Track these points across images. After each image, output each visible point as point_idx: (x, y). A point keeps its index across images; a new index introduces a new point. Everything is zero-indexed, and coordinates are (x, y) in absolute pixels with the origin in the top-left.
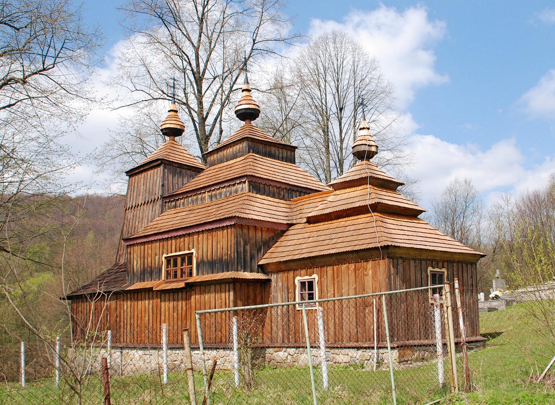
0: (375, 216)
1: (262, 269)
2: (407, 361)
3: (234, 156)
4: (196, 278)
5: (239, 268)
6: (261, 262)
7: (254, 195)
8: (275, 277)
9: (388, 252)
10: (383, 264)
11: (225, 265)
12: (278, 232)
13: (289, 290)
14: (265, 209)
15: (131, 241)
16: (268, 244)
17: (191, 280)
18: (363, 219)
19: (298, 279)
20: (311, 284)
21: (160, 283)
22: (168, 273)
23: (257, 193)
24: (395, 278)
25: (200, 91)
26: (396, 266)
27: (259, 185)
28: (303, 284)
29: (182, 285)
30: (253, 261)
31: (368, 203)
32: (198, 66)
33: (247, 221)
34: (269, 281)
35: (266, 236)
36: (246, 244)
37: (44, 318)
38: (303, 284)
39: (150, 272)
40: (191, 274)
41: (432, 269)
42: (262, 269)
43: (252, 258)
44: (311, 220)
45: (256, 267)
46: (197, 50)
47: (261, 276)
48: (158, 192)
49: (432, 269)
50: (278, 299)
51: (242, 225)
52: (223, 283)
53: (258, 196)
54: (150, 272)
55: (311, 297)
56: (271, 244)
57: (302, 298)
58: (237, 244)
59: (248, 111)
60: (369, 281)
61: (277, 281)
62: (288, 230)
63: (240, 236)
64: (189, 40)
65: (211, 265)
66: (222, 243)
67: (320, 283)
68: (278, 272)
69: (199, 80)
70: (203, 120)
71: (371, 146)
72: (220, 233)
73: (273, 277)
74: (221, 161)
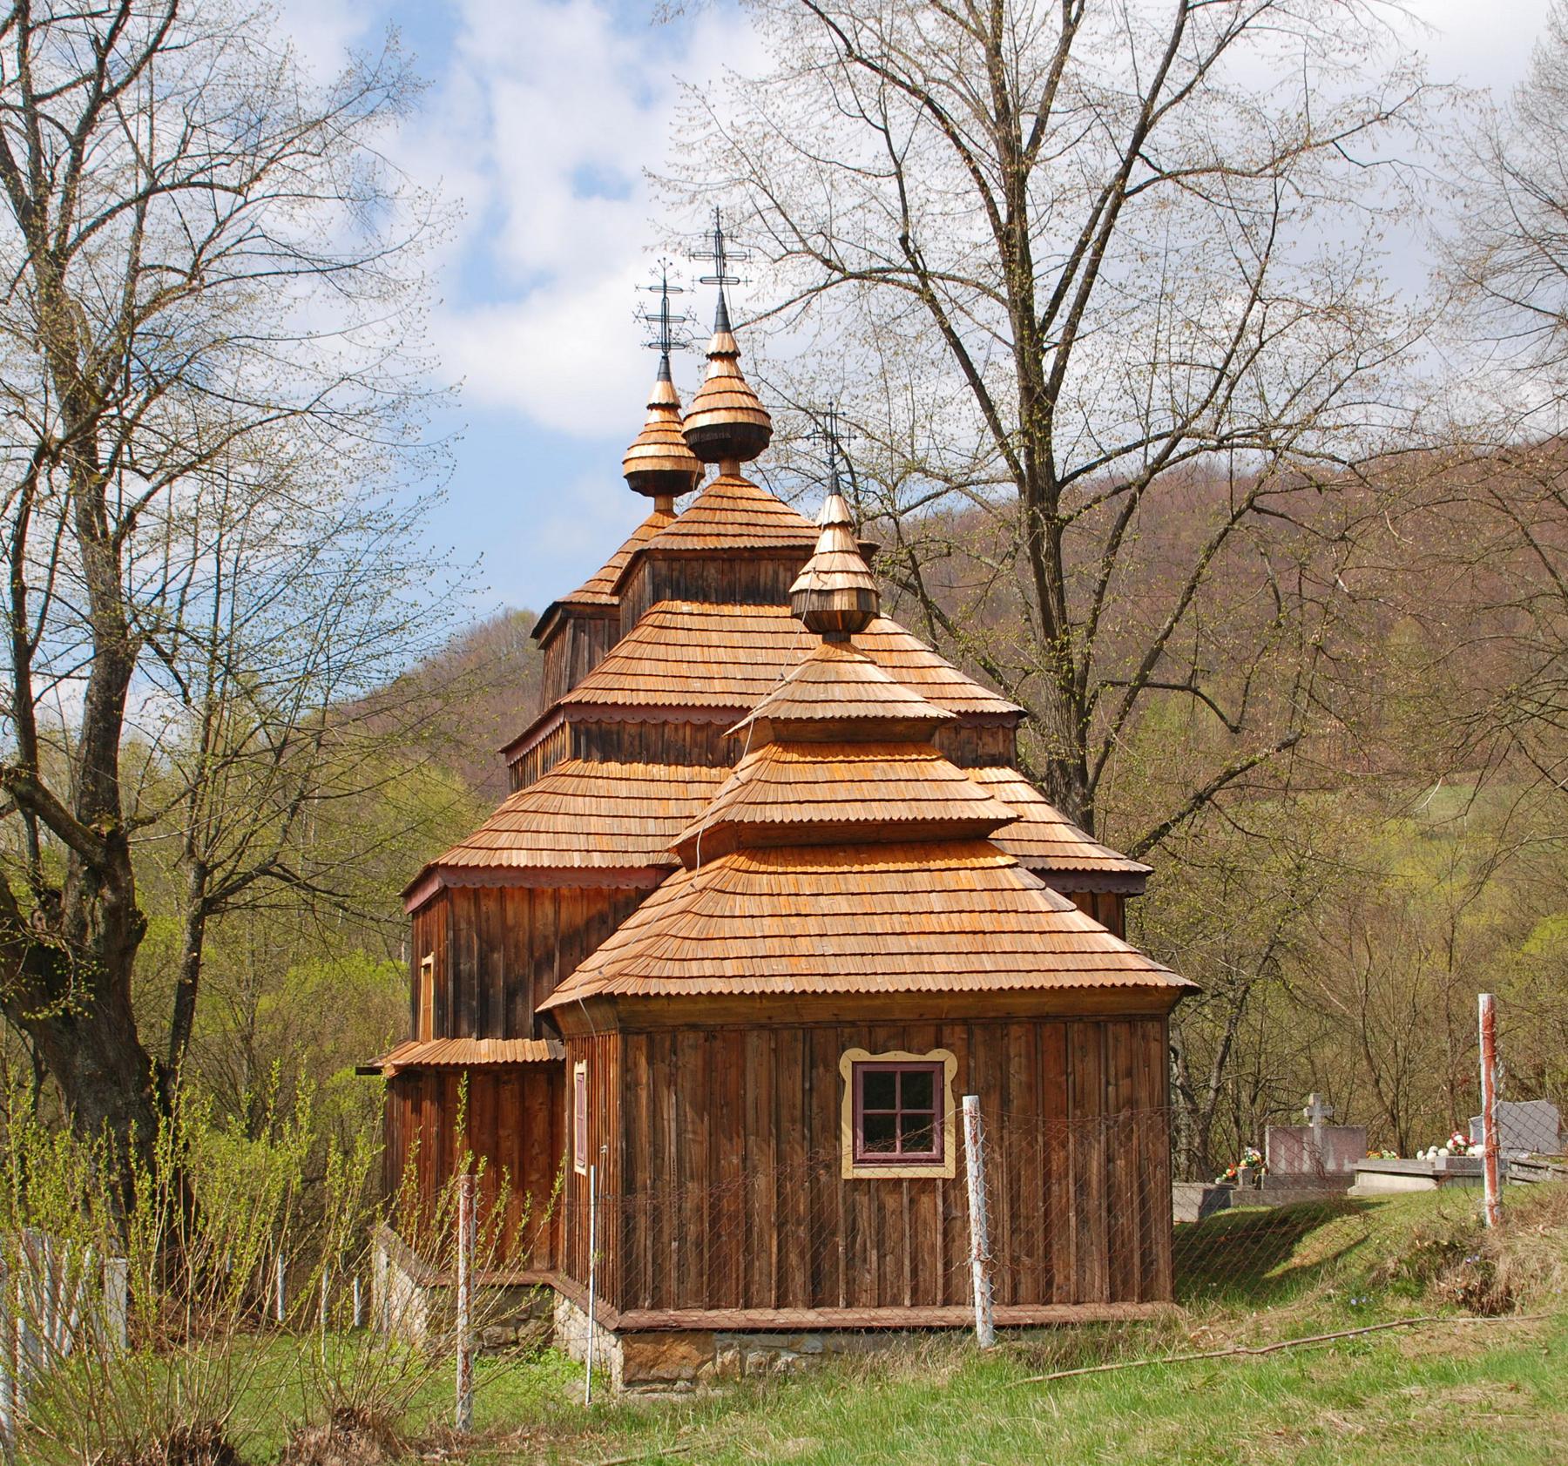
2: (673, 1381)
5: (464, 1027)
7: (595, 767)
12: (612, 898)
16: (579, 944)
23: (604, 760)
24: (655, 1100)
30: (519, 1000)
33: (486, 876)
35: (573, 914)
36: (488, 946)
41: (865, 1056)
43: (512, 994)
45: (531, 1021)
49: (865, 1056)
53: (614, 768)
56: (594, 940)
59: (708, 437)
62: (658, 887)
63: (469, 922)
71: (831, 592)
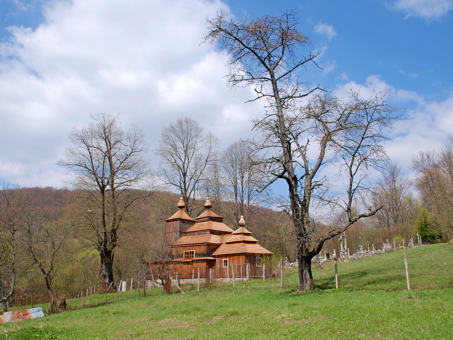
0: (243, 244)
1: (214, 256)
3: (205, 221)
4: (195, 258)
6: (213, 255)
8: (32, 314)
9: (245, 254)
10: (244, 257)
11: (203, 255)
12: (217, 246)
13: (221, 262)
14: (215, 239)
15: (172, 246)
16: (215, 249)
17: (193, 259)
18: (240, 244)
19: (223, 260)
20: (227, 261)
21: (183, 260)
22: (185, 257)
25: (185, 181)
26: (247, 257)
27: (213, 232)
28: (224, 261)
29: (191, 260)
31: (241, 240)
32: (184, 170)
34: (215, 260)
37: (362, 237)
38: (224, 261)
39: (180, 256)
40: (193, 257)
42: (214, 256)
43: (211, 253)
44: (227, 243)
46: (184, 164)
47: (213, 258)
48: (178, 229)
50: (218, 265)
51: (209, 245)
52: (234, 256)
54: (180, 256)
55: (227, 265)
57: (224, 265)
58: (207, 250)
60: (241, 261)
61: (217, 260)
64: (181, 159)
65: (198, 255)
66: (203, 249)
67: (229, 261)
68: (218, 257)
69: (185, 175)
70: (186, 190)
72: (202, 246)
73: (217, 259)
74: (200, 222)
